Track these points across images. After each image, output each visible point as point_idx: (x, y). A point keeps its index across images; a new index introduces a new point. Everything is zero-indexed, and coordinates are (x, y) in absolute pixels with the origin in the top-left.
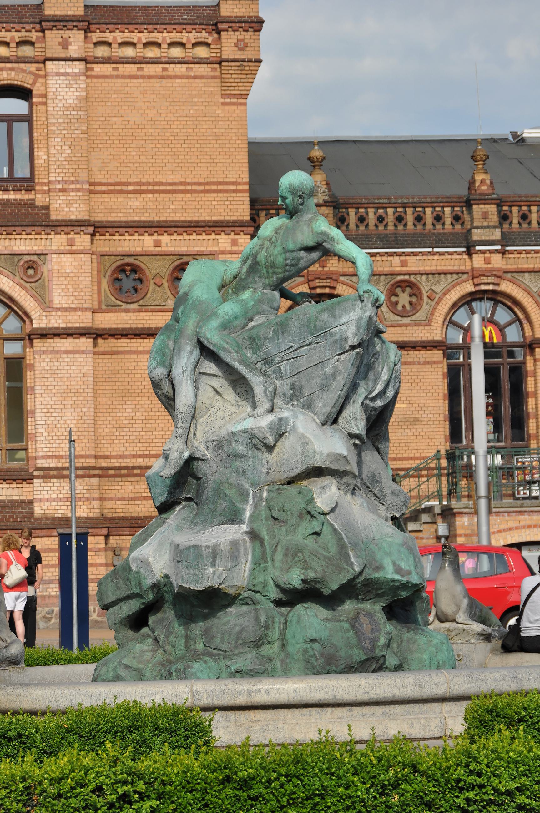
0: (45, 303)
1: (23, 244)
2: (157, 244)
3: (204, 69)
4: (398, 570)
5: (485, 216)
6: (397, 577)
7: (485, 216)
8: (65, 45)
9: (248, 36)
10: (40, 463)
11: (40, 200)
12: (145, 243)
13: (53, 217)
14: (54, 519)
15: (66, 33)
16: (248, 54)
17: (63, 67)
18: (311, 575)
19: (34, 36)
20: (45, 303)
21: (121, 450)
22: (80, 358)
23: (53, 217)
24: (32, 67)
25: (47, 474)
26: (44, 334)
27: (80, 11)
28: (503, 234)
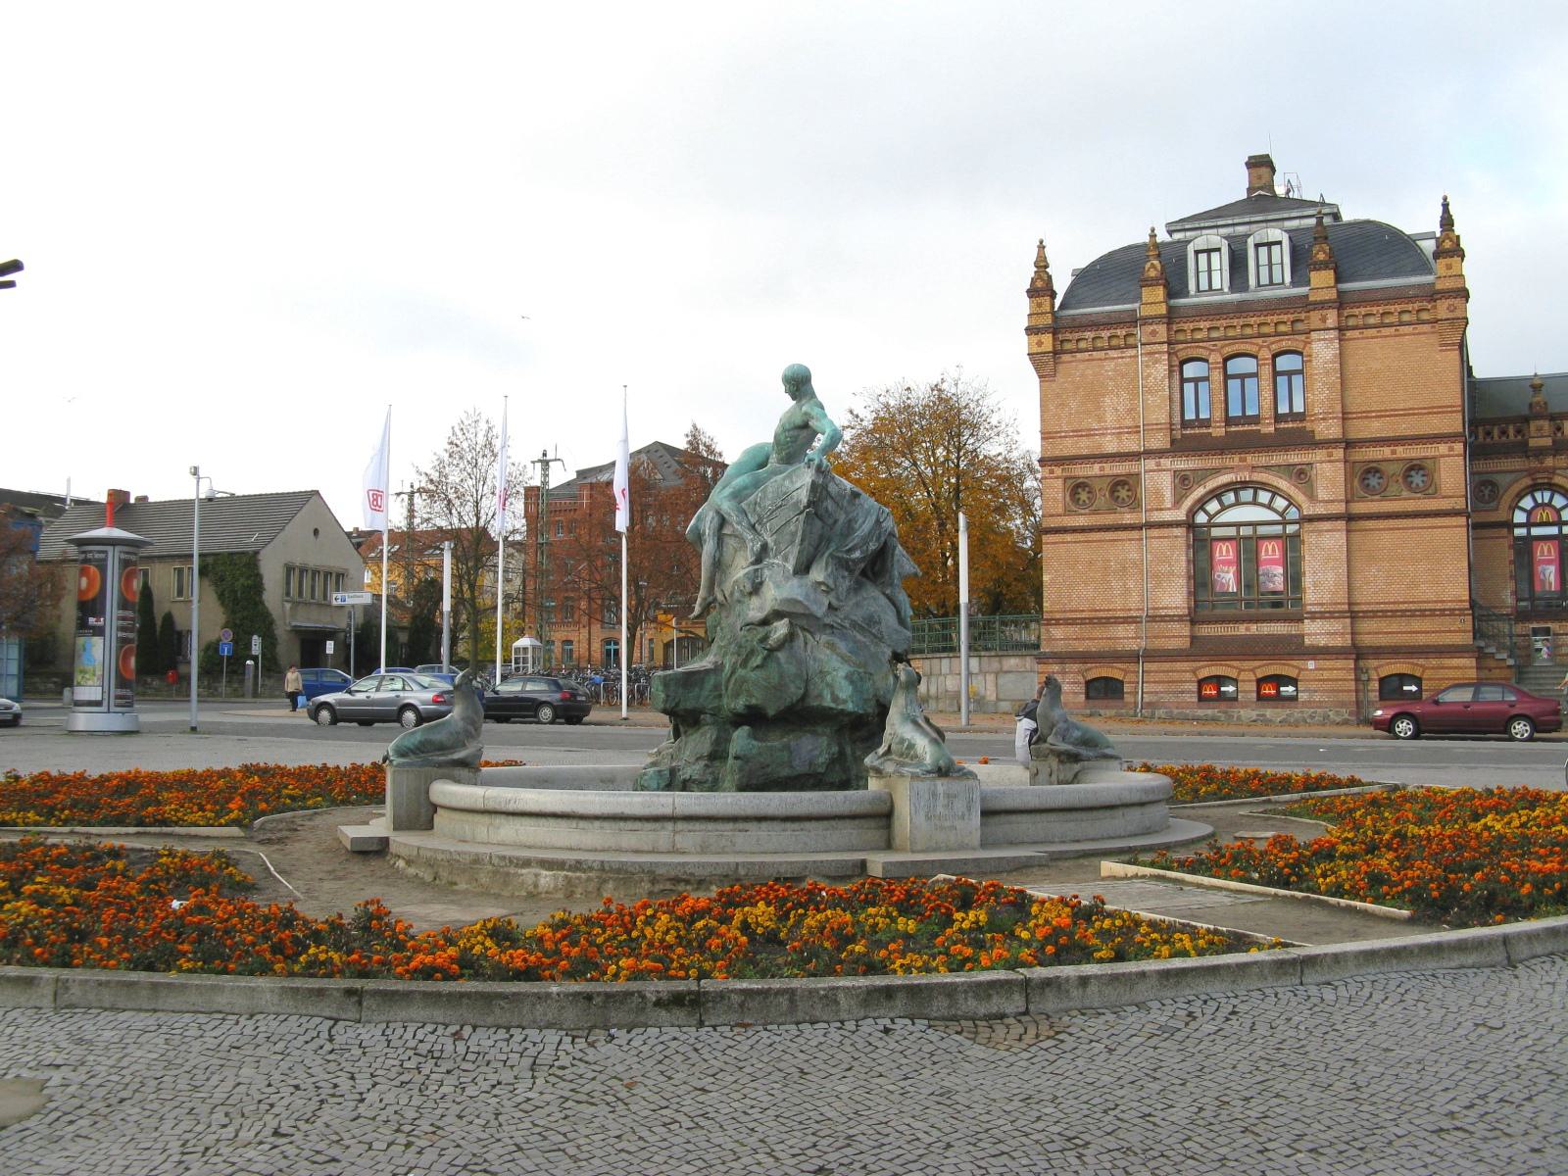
0: (1312, 497)
1: (1295, 458)
2: (1394, 452)
3: (1426, 328)
4: (835, 699)
5: (1539, 429)
6: (833, 705)
7: (1539, 429)
8: (1324, 320)
9: (1457, 302)
10: (1309, 608)
11: (1308, 426)
12: (1386, 452)
13: (1317, 438)
14: (1318, 647)
15: (1324, 312)
16: (1458, 314)
17: (1322, 335)
18: (754, 701)
19: (1303, 316)
20: (1312, 497)
21: (1369, 599)
22: (1337, 535)
23: (1317, 438)
24: (1303, 337)
25: (1314, 616)
26: (1311, 519)
27: (103, 499)
28: (1554, 442)
